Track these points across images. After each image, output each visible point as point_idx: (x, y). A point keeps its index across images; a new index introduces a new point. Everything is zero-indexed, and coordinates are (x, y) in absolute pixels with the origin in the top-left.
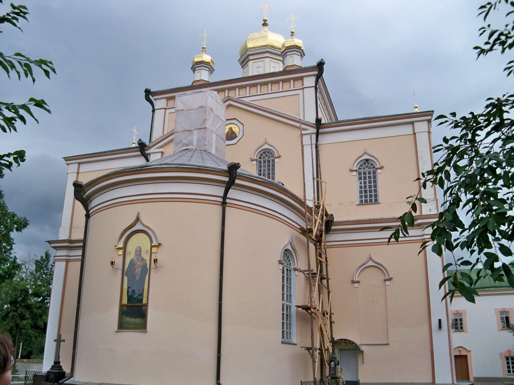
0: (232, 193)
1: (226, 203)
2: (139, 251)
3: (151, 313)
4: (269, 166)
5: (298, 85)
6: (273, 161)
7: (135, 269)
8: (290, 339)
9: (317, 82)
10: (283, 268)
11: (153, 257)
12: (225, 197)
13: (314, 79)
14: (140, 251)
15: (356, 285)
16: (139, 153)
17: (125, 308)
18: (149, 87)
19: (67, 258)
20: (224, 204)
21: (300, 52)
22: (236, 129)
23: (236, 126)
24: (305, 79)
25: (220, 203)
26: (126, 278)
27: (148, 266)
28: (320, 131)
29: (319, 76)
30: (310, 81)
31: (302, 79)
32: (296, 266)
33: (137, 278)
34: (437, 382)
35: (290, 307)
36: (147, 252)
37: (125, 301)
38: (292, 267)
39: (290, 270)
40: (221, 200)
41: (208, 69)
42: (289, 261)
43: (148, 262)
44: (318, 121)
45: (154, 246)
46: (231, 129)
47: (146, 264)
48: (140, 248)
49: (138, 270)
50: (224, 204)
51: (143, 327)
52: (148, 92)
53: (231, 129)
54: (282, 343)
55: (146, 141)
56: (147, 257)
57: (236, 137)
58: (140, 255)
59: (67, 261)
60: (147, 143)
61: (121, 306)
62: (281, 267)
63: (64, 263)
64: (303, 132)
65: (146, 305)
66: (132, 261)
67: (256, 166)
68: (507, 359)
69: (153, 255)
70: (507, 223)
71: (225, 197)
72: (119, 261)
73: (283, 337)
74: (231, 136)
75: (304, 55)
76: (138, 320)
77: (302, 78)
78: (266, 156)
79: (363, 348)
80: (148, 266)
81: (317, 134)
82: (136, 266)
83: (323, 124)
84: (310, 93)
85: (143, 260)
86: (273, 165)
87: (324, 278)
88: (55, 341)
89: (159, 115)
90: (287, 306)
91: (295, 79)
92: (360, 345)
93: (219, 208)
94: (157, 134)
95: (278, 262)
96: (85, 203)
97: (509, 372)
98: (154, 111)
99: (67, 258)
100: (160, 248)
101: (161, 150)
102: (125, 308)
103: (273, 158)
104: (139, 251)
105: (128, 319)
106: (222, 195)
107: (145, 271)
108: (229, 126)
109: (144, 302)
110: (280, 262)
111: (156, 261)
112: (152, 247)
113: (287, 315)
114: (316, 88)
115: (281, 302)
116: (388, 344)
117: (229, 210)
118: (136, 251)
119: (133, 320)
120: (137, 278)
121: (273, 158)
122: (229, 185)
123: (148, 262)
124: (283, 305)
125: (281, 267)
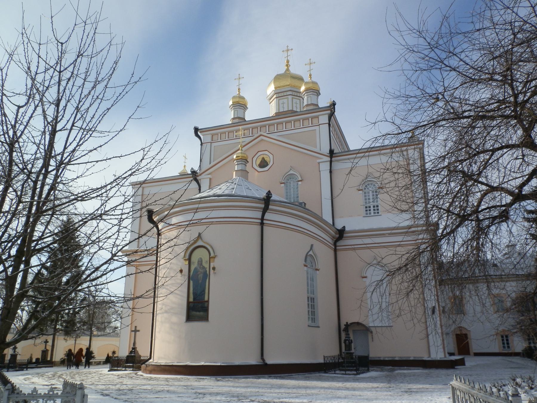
1: (264, 224)
2: (200, 262)
7: (198, 275)
9: (330, 119)
11: (212, 266)
12: (262, 219)
13: (326, 117)
14: (202, 261)
15: (364, 279)
17: (191, 305)
18: (197, 126)
20: (262, 224)
24: (320, 117)
26: (191, 282)
27: (208, 272)
29: (332, 115)
30: (324, 119)
33: (200, 282)
36: (207, 262)
37: (191, 300)
43: (208, 270)
44: (331, 152)
45: (212, 257)
46: (263, 158)
47: (206, 271)
48: (201, 258)
49: (201, 276)
50: (262, 224)
51: (205, 318)
52: (196, 130)
53: (263, 158)
55: (196, 168)
56: (207, 266)
57: (267, 165)
58: (201, 264)
61: (188, 303)
64: (319, 161)
65: (208, 301)
66: (196, 269)
68: (502, 337)
71: (262, 219)
72: (186, 271)
74: (263, 164)
75: (320, 94)
76: (202, 313)
77: (317, 117)
79: (373, 329)
80: (208, 272)
81: (331, 162)
82: (199, 273)
83: (336, 153)
85: (204, 268)
87: (492, 77)
88: (138, 331)
90: (311, 298)
93: (258, 228)
97: (504, 347)
98: (202, 144)
101: (210, 176)
104: (200, 262)
105: (194, 313)
106: (260, 217)
107: (206, 276)
109: (206, 299)
111: (214, 269)
114: (329, 125)
117: (265, 227)
118: (198, 261)
119: (198, 313)
120: (200, 282)
122: (265, 210)
123: (208, 270)
124: (308, 298)
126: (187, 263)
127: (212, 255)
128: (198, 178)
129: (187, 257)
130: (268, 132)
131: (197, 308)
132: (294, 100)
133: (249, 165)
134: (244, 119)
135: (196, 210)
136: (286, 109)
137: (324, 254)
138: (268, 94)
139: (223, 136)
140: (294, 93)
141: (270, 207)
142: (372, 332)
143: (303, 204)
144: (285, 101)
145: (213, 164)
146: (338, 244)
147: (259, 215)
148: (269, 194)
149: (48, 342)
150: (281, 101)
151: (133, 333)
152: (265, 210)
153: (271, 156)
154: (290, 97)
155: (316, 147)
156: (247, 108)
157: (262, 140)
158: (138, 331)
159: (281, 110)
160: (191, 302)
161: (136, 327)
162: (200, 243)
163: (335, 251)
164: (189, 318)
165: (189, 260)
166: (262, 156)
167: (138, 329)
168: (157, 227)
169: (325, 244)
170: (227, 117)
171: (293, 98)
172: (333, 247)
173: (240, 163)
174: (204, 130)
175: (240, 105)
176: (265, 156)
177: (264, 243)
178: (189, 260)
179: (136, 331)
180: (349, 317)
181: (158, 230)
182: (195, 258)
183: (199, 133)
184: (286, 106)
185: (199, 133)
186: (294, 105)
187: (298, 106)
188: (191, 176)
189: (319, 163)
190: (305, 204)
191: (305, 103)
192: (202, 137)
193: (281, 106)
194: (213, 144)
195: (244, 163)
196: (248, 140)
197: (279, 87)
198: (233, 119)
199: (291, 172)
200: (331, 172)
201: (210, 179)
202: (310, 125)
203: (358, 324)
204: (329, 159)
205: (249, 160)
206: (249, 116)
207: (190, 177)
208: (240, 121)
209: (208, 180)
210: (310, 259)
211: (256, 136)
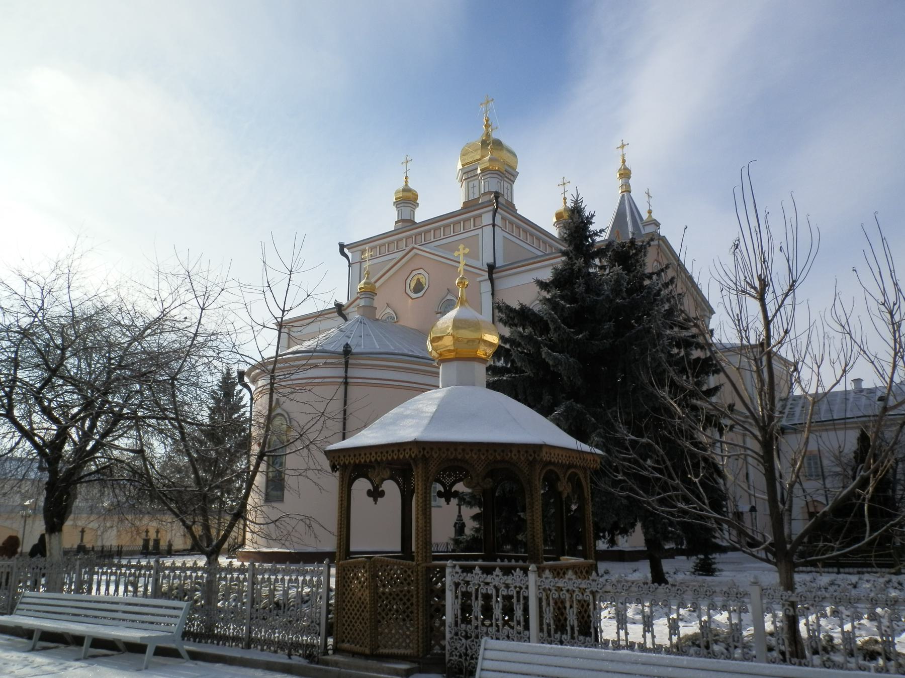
20: (346, 383)
46: (418, 280)
50: (346, 383)
52: (342, 247)
53: (418, 280)
55: (344, 301)
64: (478, 279)
135: (310, 358)
139: (400, 243)
148: (347, 346)
149: (370, 493)
150: (471, 184)
153: (427, 276)
157: (416, 254)
166: (416, 278)
170: (385, 220)
174: (351, 246)
175: (407, 199)
176: (420, 276)
185: (346, 250)
189: (480, 282)
192: (350, 255)
196: (399, 255)
197: (467, 164)
198: (396, 222)
199: (449, 297)
206: (421, 215)
208: (406, 223)
211: (408, 249)
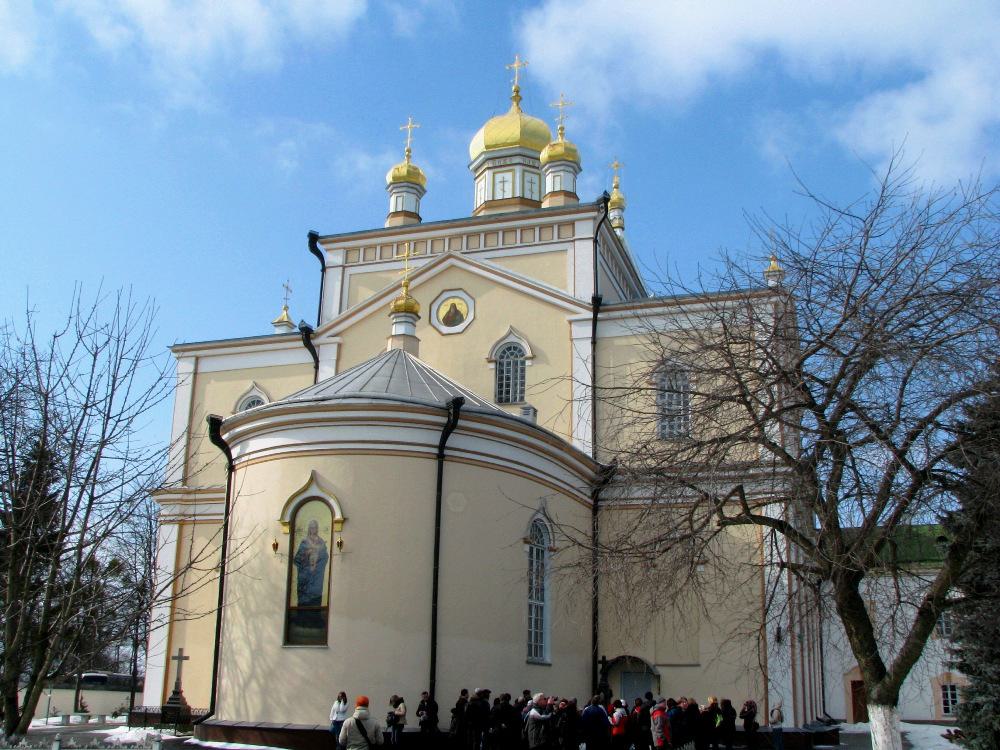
0: (454, 440)
3: (335, 623)
4: (516, 371)
5: (566, 232)
6: (523, 363)
8: (541, 656)
10: (531, 549)
14: (317, 527)
16: (301, 343)
18: (315, 229)
19: (182, 518)
21: (572, 167)
22: (461, 308)
23: (462, 302)
25: (435, 456)
26: (295, 569)
28: (599, 316)
30: (585, 229)
31: (573, 224)
32: (552, 545)
34: (128, 694)
35: (542, 608)
37: (294, 603)
38: (547, 544)
39: (543, 552)
40: (436, 451)
41: (415, 191)
42: (542, 536)
43: (328, 545)
45: (337, 522)
46: (454, 306)
52: (313, 238)
53: (454, 306)
54: (528, 662)
55: (312, 323)
56: (325, 537)
57: (461, 320)
58: (316, 534)
59: (182, 524)
60: (315, 328)
61: (289, 610)
62: (527, 548)
63: (176, 527)
65: (327, 609)
67: (494, 372)
68: (944, 688)
69: (335, 534)
70: (492, 706)
71: (442, 446)
73: (530, 654)
74: (454, 317)
76: (315, 631)
77: (572, 223)
78: (512, 354)
79: (661, 671)
81: (595, 321)
83: (605, 305)
84: (585, 250)
85: (320, 542)
86: (523, 370)
88: (187, 658)
89: (334, 279)
91: (560, 225)
92: (654, 666)
93: (434, 464)
94: (332, 311)
95: (522, 542)
96: (225, 447)
97: (946, 710)
98: (324, 270)
99: (182, 518)
100: (347, 526)
102: (294, 614)
103: (522, 359)
104: (313, 530)
105: (300, 630)
106: (437, 443)
108: (451, 301)
109: (324, 603)
110: (526, 541)
112: (334, 522)
113: (536, 621)
114: (596, 241)
115: (525, 602)
116: (698, 665)
117: (447, 465)
121: (522, 359)
122: (448, 430)
123: (328, 545)
124: (530, 606)
125: (527, 548)
126: (287, 529)
127: (338, 516)
128: (314, 342)
129: (287, 520)
130: (464, 250)
131: (305, 621)
132: (528, 176)
133: (422, 322)
134: (416, 216)
136: (508, 195)
137: (571, 515)
138: (473, 156)
140: (527, 161)
141: (461, 423)
142: (658, 677)
143: (531, 411)
144: (508, 176)
145: (345, 313)
146: (602, 495)
147: (434, 438)
150: (499, 177)
151: (176, 662)
152: (448, 430)
154: (518, 169)
155: (565, 287)
156: (425, 191)
157: (452, 266)
158: (187, 658)
159: (499, 196)
160: (294, 608)
161: (181, 650)
162: (314, 491)
163: (595, 510)
164: (290, 639)
165: (292, 524)
167: (185, 654)
168: (228, 453)
169: (575, 498)
171: (524, 171)
172: (591, 501)
173: (403, 319)
174: (327, 240)
176: (456, 301)
177: (434, 525)
178: (292, 524)
179: (181, 658)
180: (609, 652)
181: (231, 460)
182: (305, 518)
183: (318, 245)
184: (508, 187)
186: (527, 186)
187: (536, 188)
188: (300, 336)
189: (570, 322)
190: (535, 411)
191: (549, 189)
193: (499, 186)
194: (349, 271)
195: (411, 320)
196: (421, 264)
200: (594, 343)
201: (340, 346)
202: (556, 240)
203: (636, 660)
204: (590, 315)
205: (423, 312)
207: (299, 340)
209: (335, 346)
210: (538, 535)
211: (441, 256)
